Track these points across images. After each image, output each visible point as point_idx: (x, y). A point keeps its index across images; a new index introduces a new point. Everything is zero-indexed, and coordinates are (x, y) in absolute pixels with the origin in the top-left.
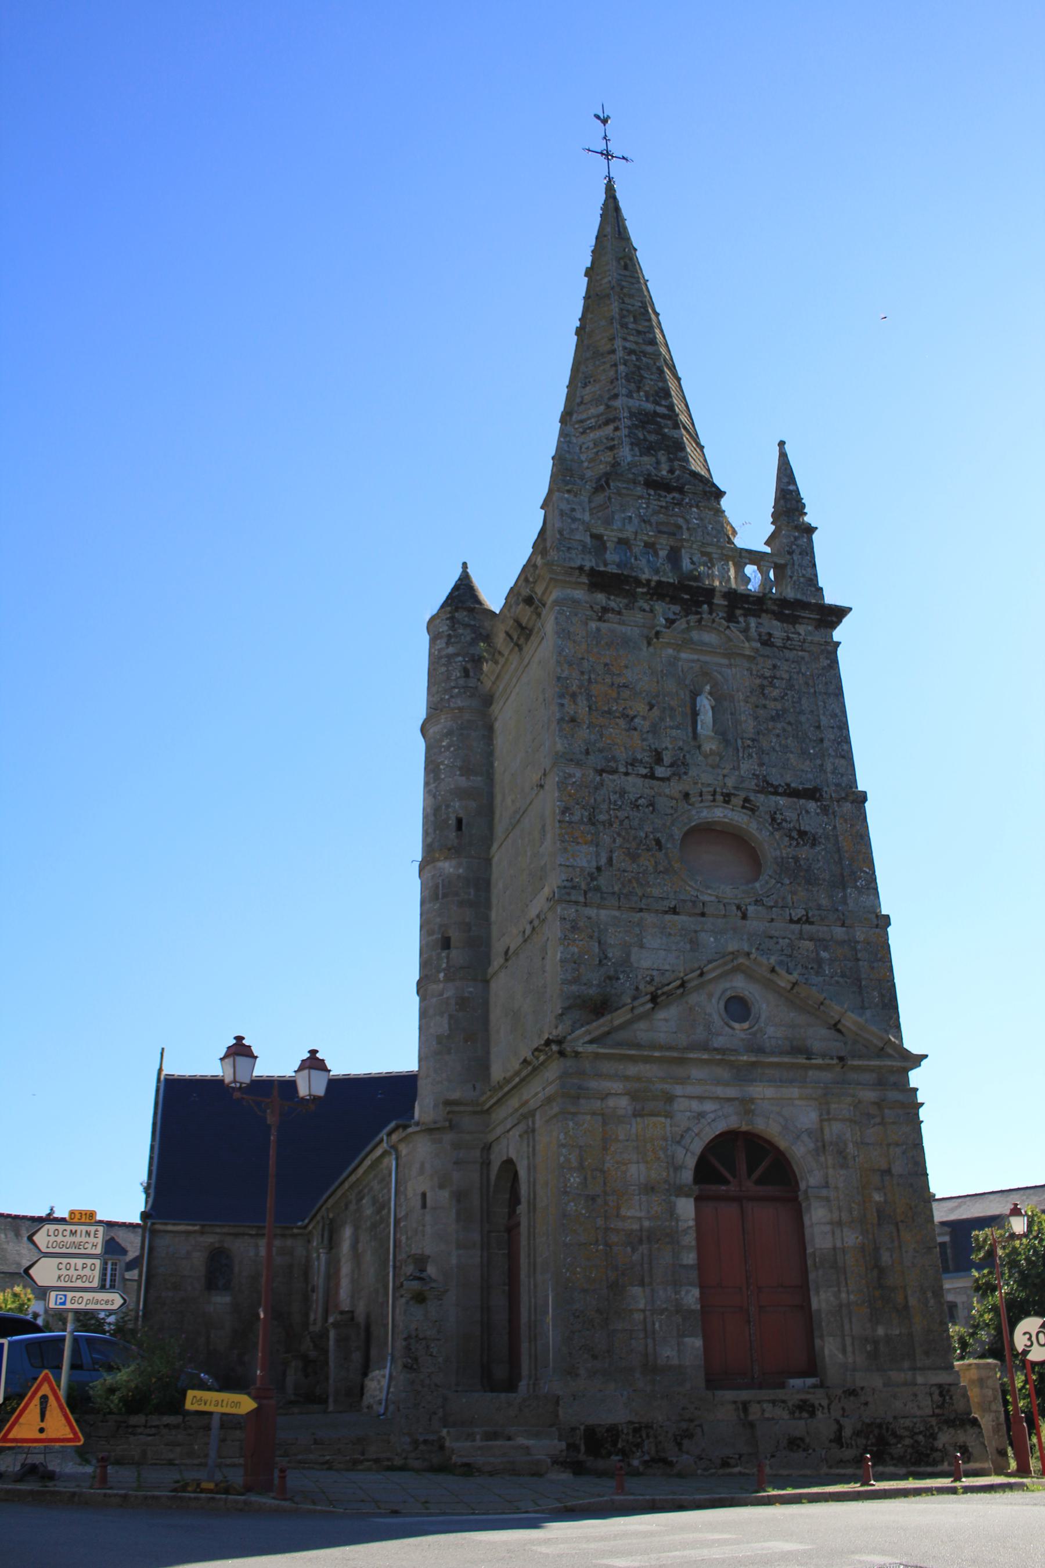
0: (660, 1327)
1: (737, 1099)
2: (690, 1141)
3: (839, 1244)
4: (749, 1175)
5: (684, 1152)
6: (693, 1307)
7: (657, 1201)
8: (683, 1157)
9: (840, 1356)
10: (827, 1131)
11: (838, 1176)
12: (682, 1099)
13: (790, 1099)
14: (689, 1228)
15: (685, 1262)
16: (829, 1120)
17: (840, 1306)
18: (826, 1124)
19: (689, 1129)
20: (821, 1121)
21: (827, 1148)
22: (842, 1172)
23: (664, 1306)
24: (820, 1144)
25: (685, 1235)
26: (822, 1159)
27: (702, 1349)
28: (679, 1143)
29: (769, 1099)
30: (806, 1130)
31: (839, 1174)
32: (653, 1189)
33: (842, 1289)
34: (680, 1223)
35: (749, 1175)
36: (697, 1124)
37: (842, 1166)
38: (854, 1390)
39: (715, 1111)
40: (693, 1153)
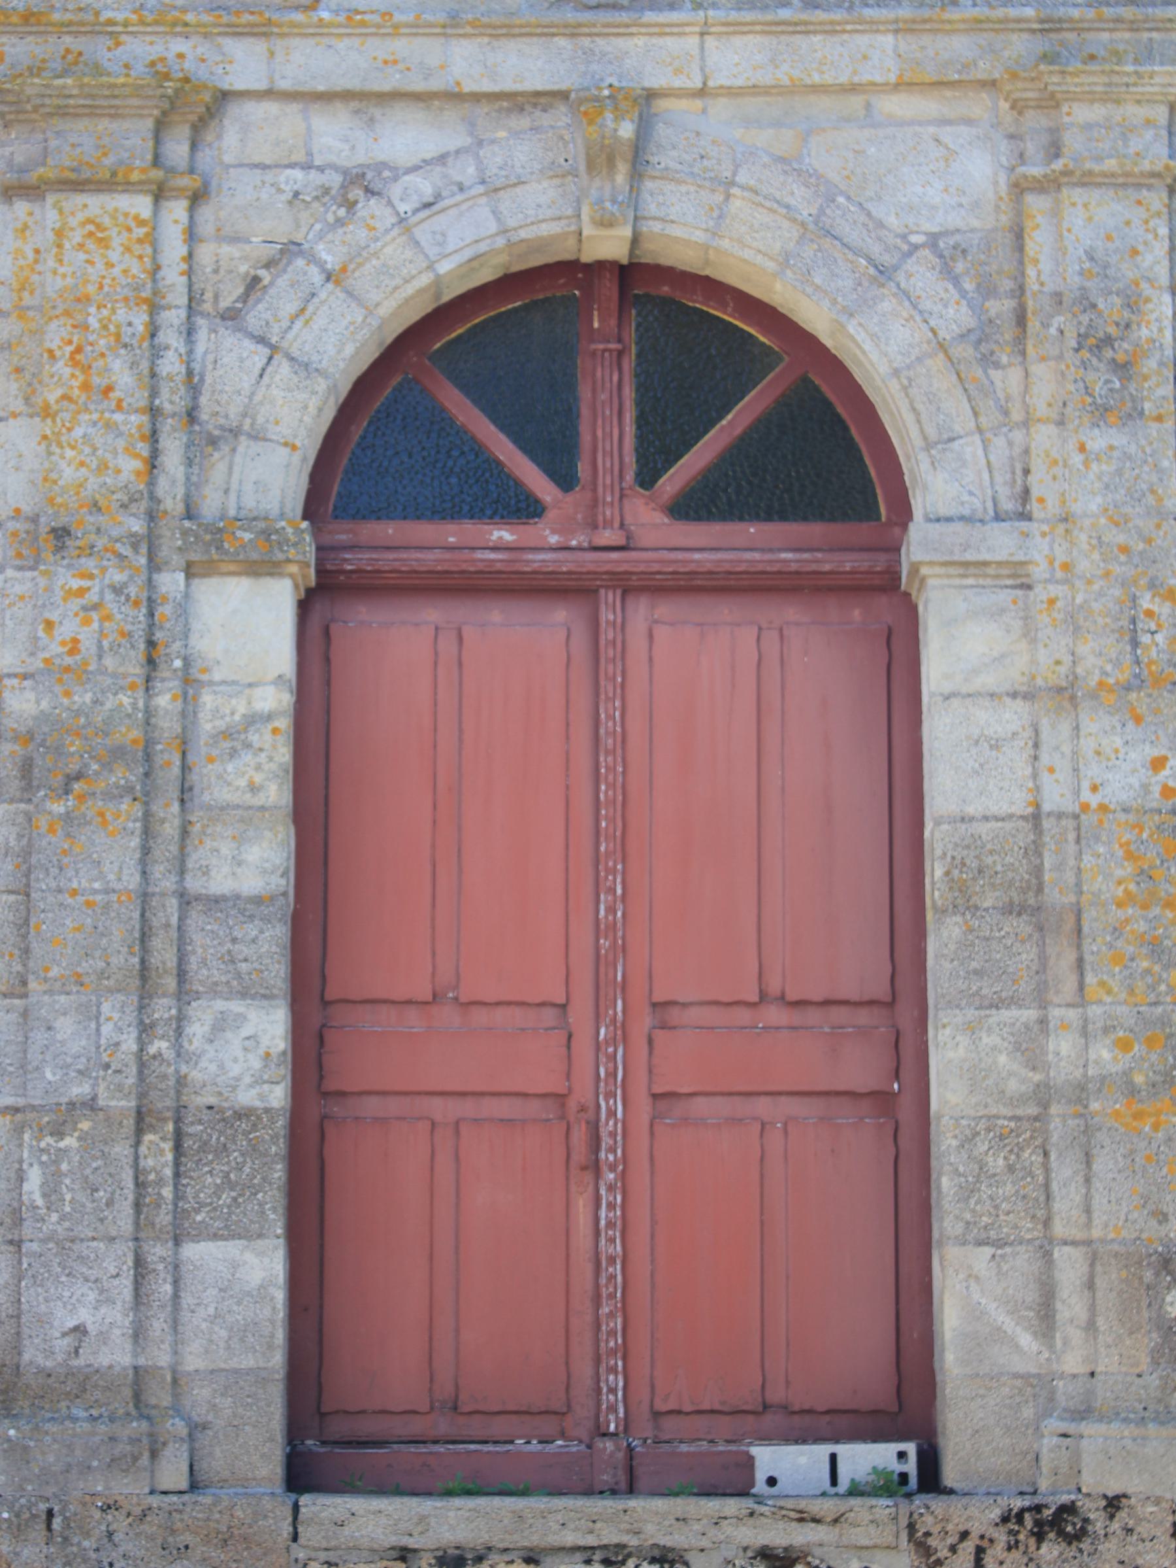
0: (51, 1191)
1: (563, 95)
2: (291, 308)
3: (1055, 797)
4: (647, 478)
5: (259, 361)
6: (247, 1097)
7: (81, 592)
8: (246, 383)
9: (1026, 1340)
10: (1039, 241)
11: (1077, 459)
12: (271, 108)
13: (853, 89)
14: (253, 720)
15: (220, 882)
16: (1048, 185)
17: (1043, 1095)
18: (1036, 203)
19: (291, 250)
20: (1019, 188)
21: (1033, 325)
22: (1098, 440)
23: (79, 1090)
24: (1001, 307)
25: (233, 754)
26: (1008, 380)
27: (280, 1296)
28: (231, 316)
29: (731, 92)
30: (933, 240)
31: (1082, 448)
32: (61, 534)
33: (1055, 1013)
34: (208, 699)
35: (647, 478)
36: (340, 222)
37: (1101, 413)
38: (1068, 1509)
39: (442, 159)
40: (303, 367)
